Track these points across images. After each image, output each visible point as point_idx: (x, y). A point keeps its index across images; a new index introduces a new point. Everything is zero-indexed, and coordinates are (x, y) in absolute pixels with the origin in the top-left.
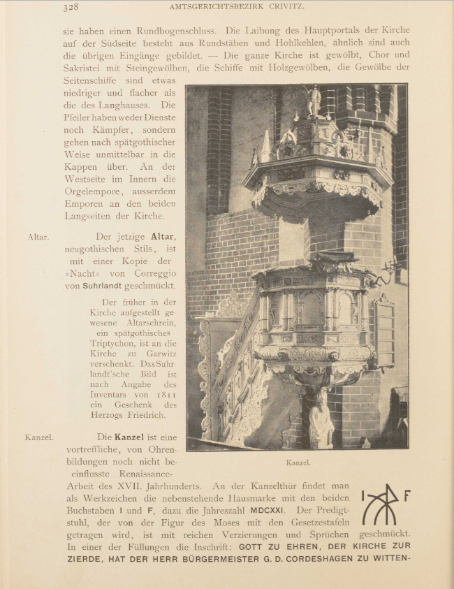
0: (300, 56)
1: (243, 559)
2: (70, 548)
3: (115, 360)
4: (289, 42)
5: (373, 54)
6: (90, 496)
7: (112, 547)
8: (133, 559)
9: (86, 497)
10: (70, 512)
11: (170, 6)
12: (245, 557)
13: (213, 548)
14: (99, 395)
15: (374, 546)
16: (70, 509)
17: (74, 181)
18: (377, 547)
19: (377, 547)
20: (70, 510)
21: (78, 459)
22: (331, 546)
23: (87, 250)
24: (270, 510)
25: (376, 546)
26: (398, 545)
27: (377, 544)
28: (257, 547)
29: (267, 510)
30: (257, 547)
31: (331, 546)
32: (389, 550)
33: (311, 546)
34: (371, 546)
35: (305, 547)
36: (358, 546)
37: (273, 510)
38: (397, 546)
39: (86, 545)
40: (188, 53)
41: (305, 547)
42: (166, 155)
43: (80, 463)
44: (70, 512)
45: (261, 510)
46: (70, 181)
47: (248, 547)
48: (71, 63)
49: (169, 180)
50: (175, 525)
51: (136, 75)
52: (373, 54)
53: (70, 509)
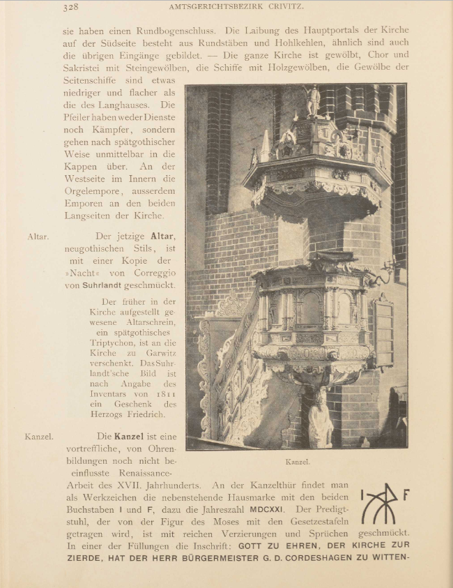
3: (115, 359)
5: (372, 54)
6: (90, 496)
8: (132, 558)
9: (86, 496)
10: (70, 511)
14: (99, 395)
15: (373, 545)
16: (70, 508)
17: (74, 180)
18: (376, 546)
19: (376, 546)
20: (70, 509)
22: (330, 546)
23: (87, 249)
24: (270, 509)
27: (376, 543)
28: (256, 546)
29: (267, 509)
30: (256, 546)
31: (330, 546)
33: (311, 545)
34: (370, 545)
35: (305, 546)
36: (357, 545)
37: (272, 509)
41: (305, 546)
43: (79, 462)
44: (70, 511)
45: (261, 509)
46: (69, 180)
47: (248, 546)
48: (71, 63)
49: (168, 179)
51: (136, 75)
52: (372, 54)
53: (70, 508)
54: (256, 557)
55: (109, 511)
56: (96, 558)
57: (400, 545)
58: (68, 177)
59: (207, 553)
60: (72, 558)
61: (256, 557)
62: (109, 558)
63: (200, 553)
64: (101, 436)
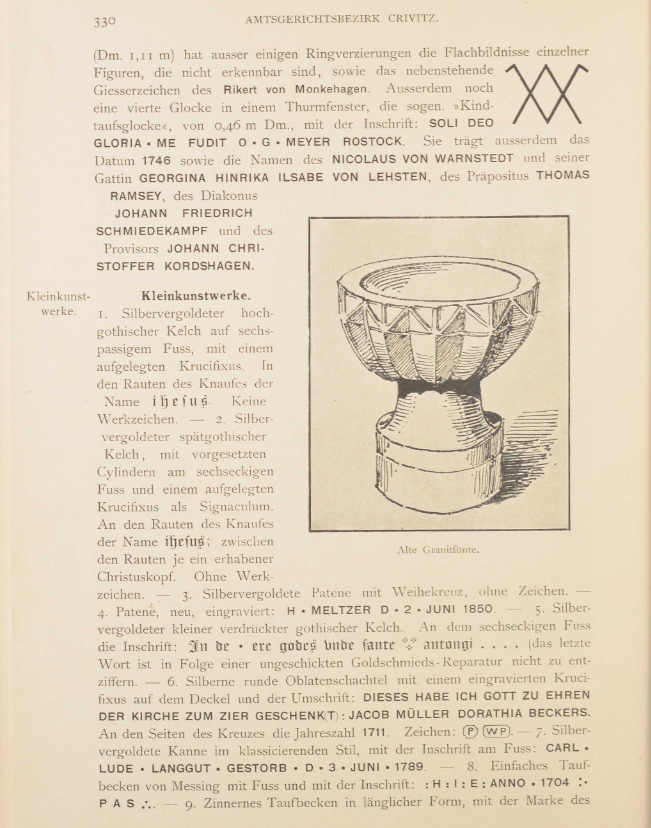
0: (112, 109)
1: (105, 266)
2: (128, 648)
4: (136, 435)
5: (104, 576)
6: (108, 662)
7: (401, 750)
8: (103, 716)
9: (103, 662)
11: (101, 731)
12: (108, 263)
13: (143, 332)
15: (243, 213)
17: (110, 422)
18: (242, 250)
19: (242, 250)
20: (104, 664)
21: (137, 626)
22: (472, 123)
23: (108, 333)
25: (115, 231)
26: (227, 715)
27: (166, 714)
28: (509, 696)
30: (509, 696)
31: (472, 123)
32: (400, 166)
33: (418, 175)
34: (157, 716)
35: (573, 695)
36: (139, 716)
38: (529, 696)
39: (100, 106)
40: (137, 626)
41: (573, 695)
42: (101, 648)
46: (104, 421)
47: (497, 696)
48: (108, 552)
49: (105, 648)
50: (113, 76)
51: (108, 100)
54: (151, 265)
55: (138, 526)
56: (423, 176)
57: (111, 770)
58: (102, 417)
59: (221, 205)
60: (226, 717)
61: (151, 265)
62: (217, 178)
63: (376, 133)
64: (207, 195)
